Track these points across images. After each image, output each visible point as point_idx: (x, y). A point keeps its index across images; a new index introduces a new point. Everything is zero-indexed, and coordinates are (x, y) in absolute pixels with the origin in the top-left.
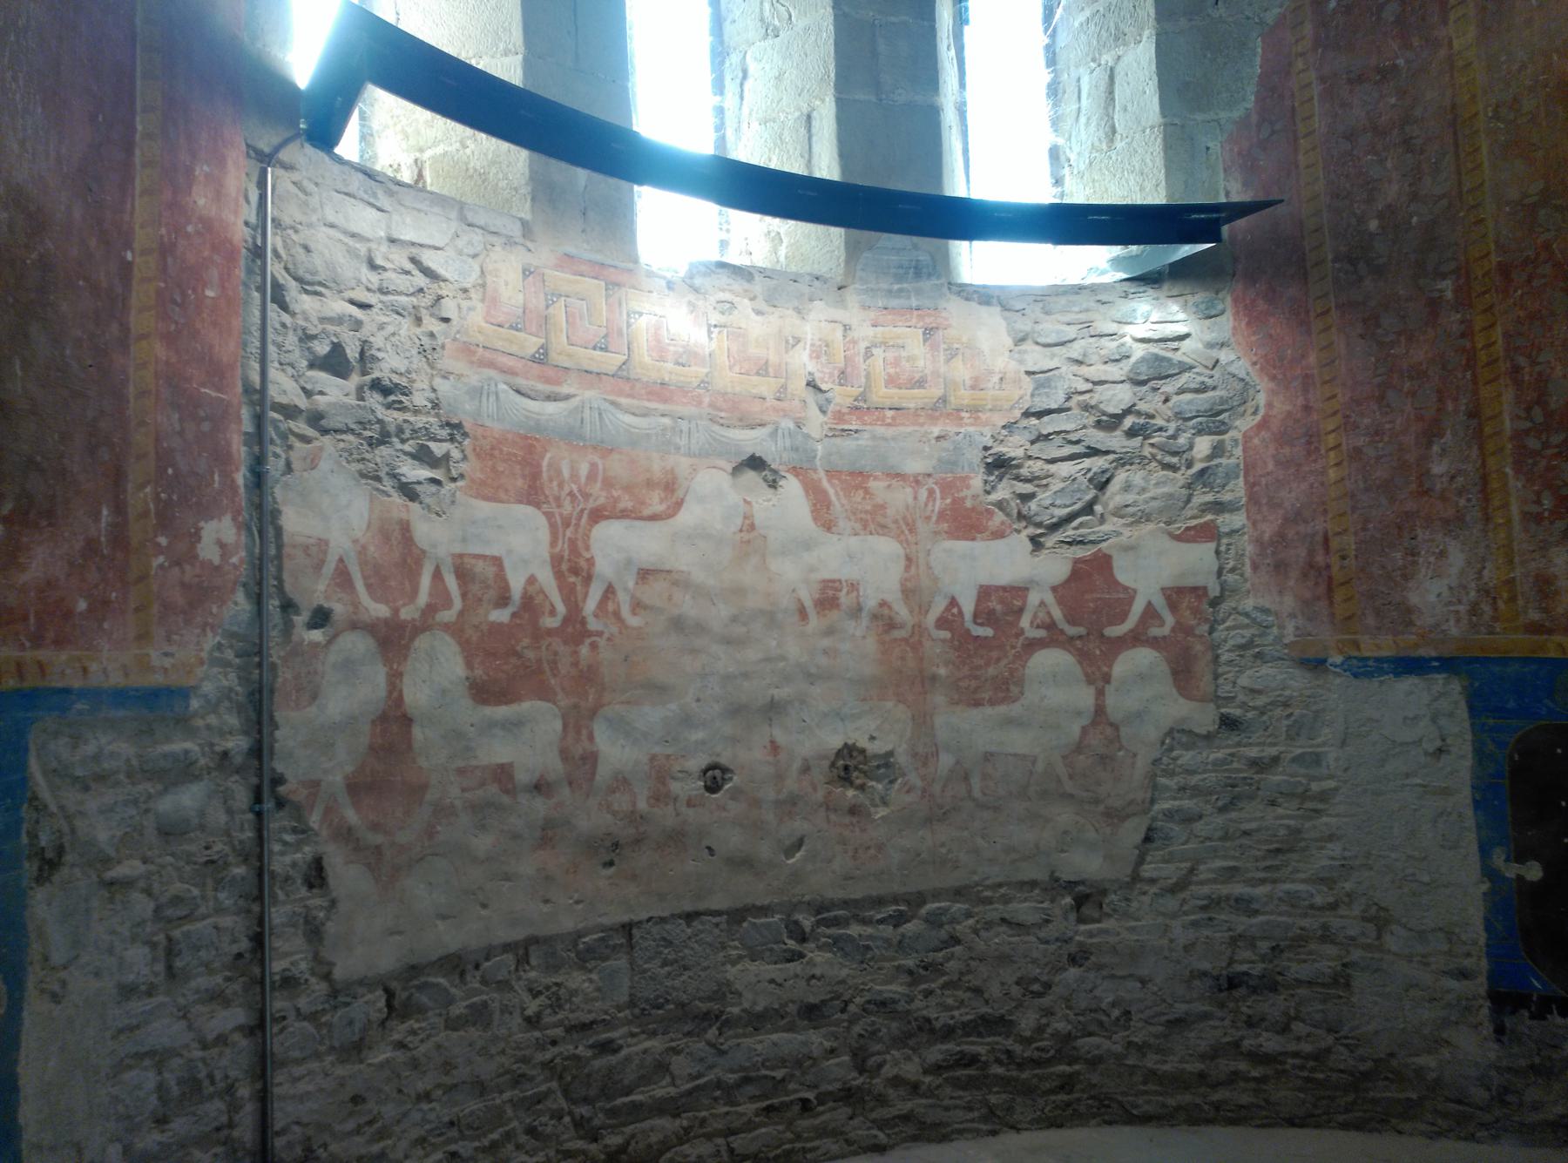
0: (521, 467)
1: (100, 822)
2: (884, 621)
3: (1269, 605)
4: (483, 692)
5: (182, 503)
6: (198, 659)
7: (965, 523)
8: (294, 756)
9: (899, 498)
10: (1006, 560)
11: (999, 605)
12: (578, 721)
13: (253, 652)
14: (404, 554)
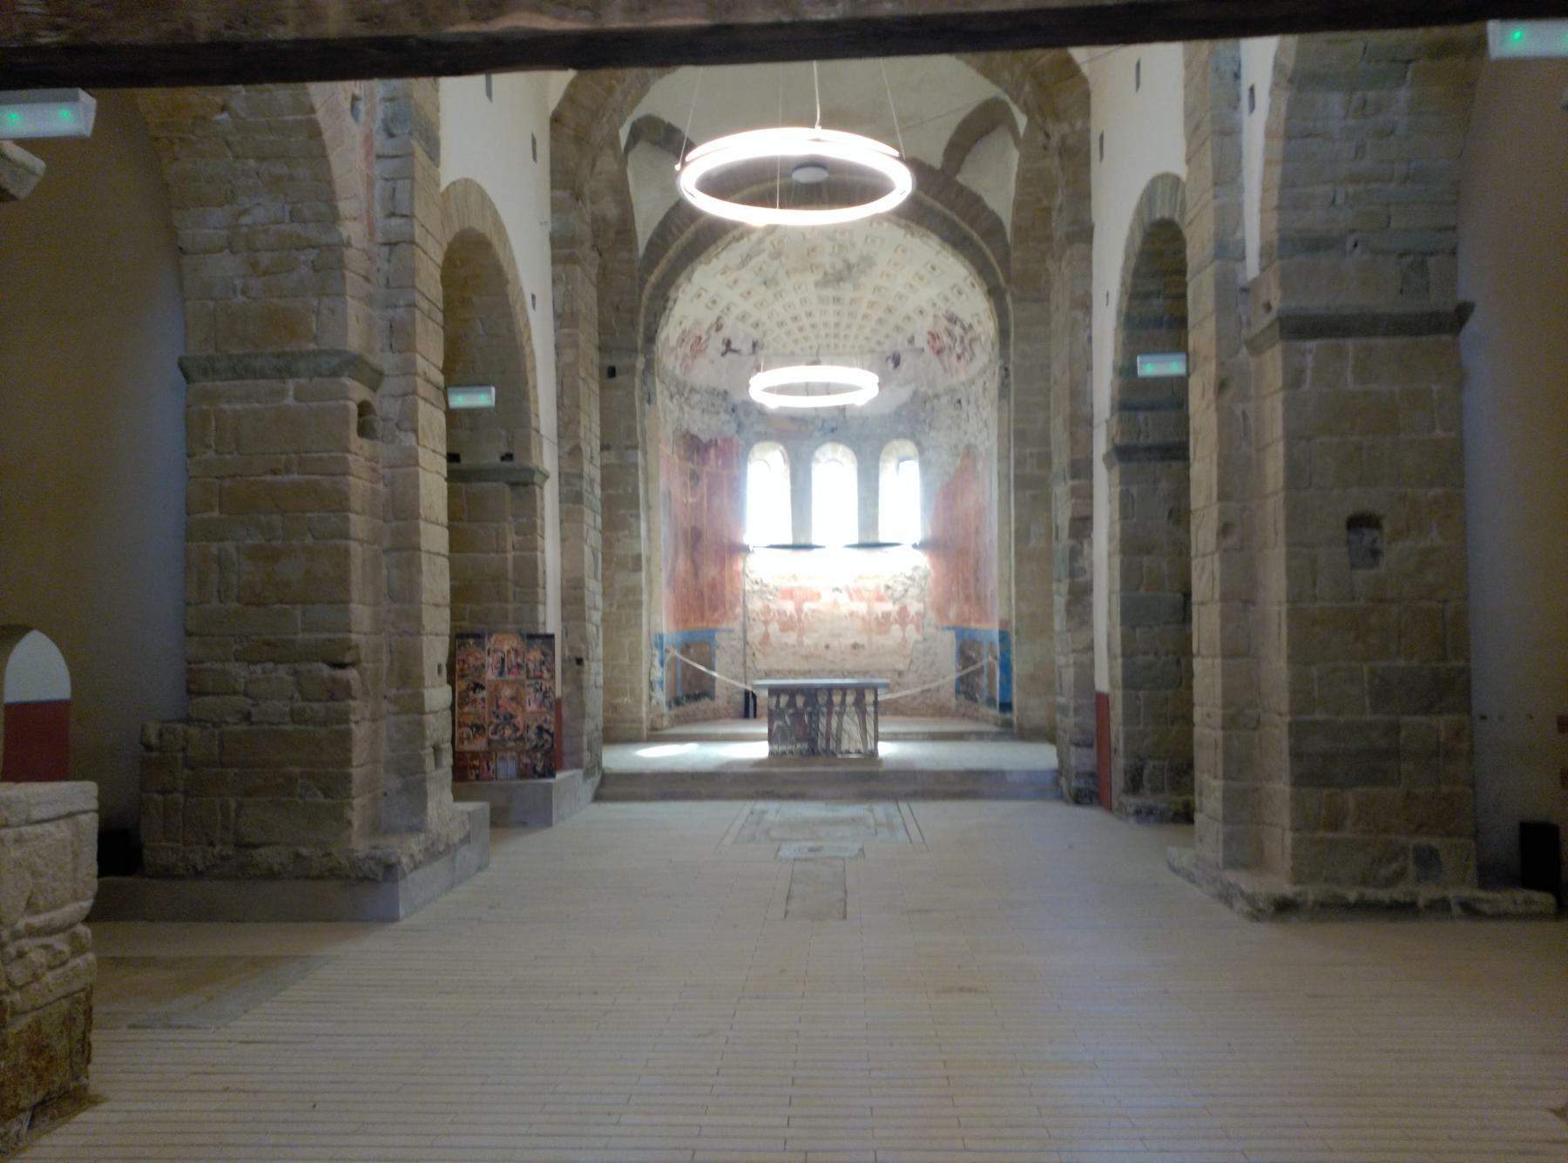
0: (789, 594)
1: (723, 644)
2: (863, 619)
3: (931, 615)
4: (782, 630)
5: (733, 606)
6: (736, 626)
7: (880, 599)
8: (750, 638)
9: (866, 595)
10: (888, 607)
11: (886, 616)
12: (800, 636)
13: (744, 624)
14: (767, 610)
